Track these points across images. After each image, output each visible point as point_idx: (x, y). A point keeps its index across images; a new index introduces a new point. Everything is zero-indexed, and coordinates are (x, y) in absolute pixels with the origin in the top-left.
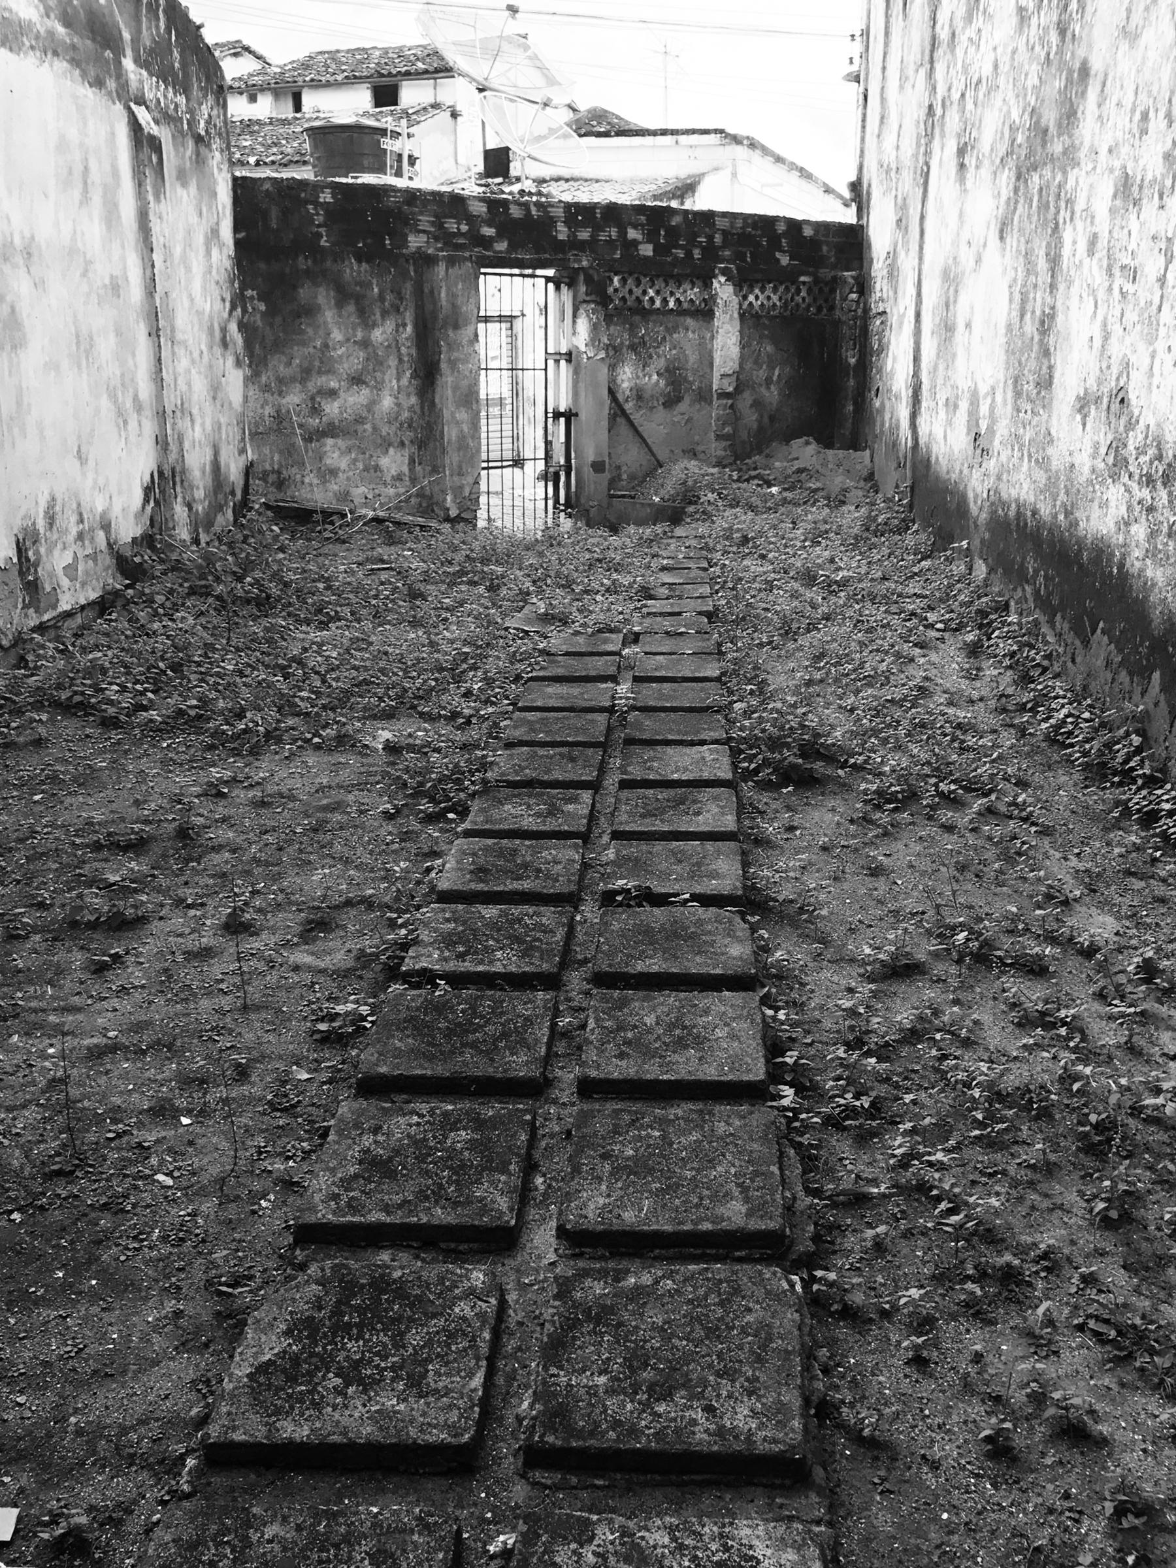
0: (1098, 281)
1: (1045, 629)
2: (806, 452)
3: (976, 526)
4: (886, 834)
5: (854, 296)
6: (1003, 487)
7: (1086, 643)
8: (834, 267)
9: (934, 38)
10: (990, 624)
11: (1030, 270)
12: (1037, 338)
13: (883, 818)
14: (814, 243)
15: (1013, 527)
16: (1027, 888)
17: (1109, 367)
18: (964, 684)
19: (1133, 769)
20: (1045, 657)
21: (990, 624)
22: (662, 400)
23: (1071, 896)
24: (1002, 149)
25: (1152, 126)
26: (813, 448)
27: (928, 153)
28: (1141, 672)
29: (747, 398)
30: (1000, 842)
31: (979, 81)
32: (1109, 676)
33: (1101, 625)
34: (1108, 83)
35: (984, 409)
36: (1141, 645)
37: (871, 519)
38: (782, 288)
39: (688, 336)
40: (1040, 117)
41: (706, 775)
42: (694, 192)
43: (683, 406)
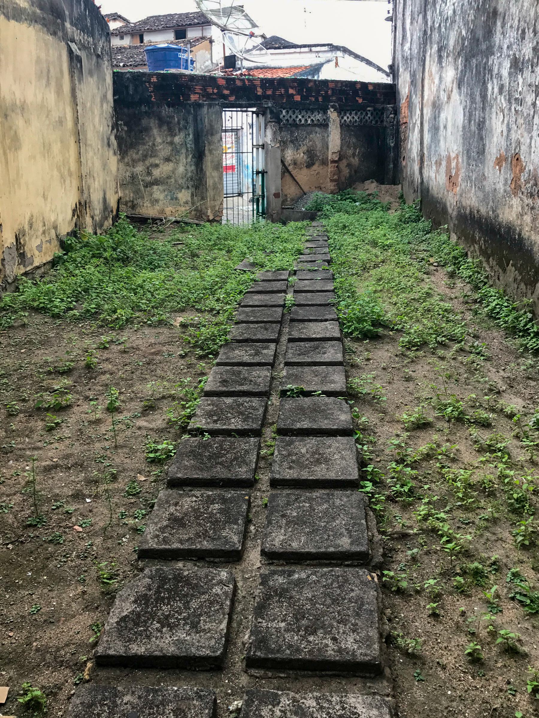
0: (504, 105)
1: (485, 264)
2: (372, 186)
3: (451, 218)
4: (412, 362)
5: (392, 116)
6: (463, 200)
7: (504, 271)
8: (383, 103)
12: (477, 132)
13: (411, 354)
14: (374, 93)
15: (469, 218)
16: (480, 386)
17: (511, 144)
18: (447, 291)
19: (528, 329)
21: (459, 263)
22: (305, 165)
23: (501, 389)
24: (458, 48)
26: (375, 184)
27: (425, 52)
29: (344, 162)
32: (516, 286)
33: (511, 262)
35: (453, 164)
38: (359, 113)
39: (316, 137)
40: (475, 33)
41: (328, 335)
43: (315, 167)
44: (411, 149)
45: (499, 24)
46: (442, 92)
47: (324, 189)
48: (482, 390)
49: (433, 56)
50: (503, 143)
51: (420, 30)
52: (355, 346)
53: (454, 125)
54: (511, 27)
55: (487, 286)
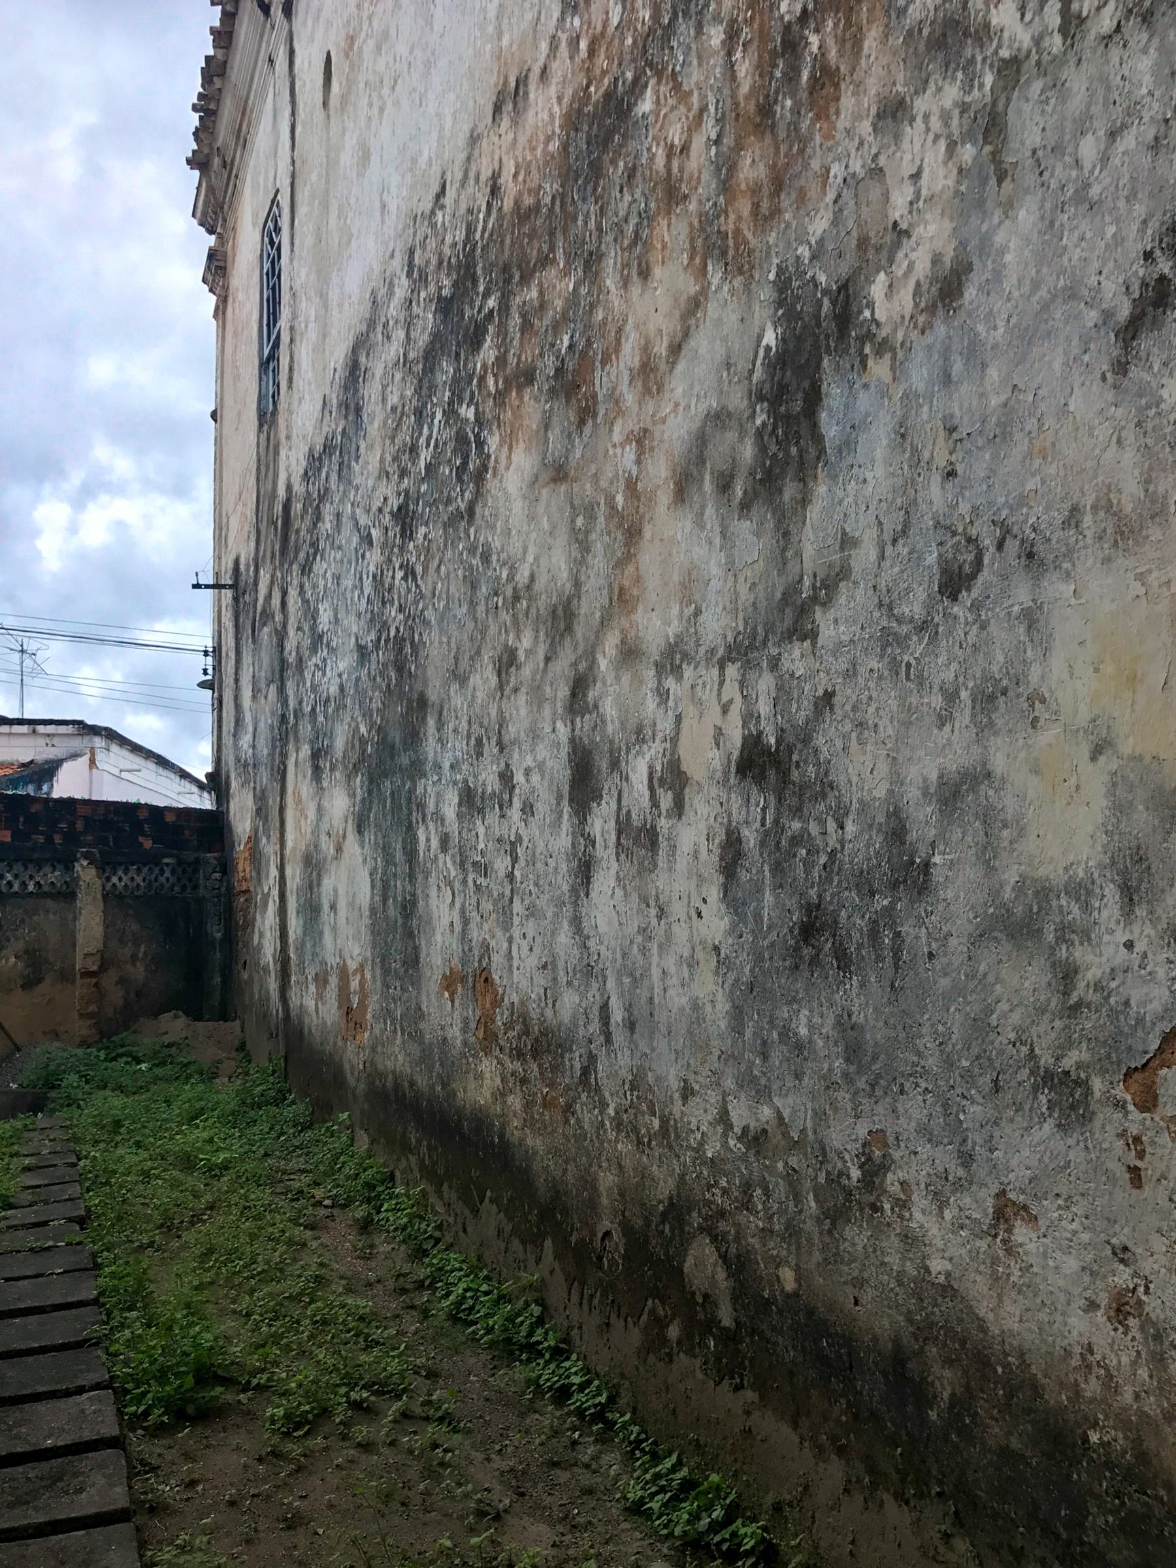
0: (453, 874)
1: (433, 1199)
2: (175, 1026)
3: (355, 1097)
4: (298, 1470)
5: (217, 875)
6: (378, 1059)
7: (476, 1212)
9: (283, 661)
11: (389, 860)
12: (400, 921)
13: (294, 1449)
17: (470, 950)
18: (359, 1265)
19: (539, 1343)
22: (20, 983)
23: (501, 1506)
24: (354, 757)
26: (182, 1020)
27: (284, 756)
28: (533, 1240)
29: (112, 975)
30: (421, 1455)
31: (328, 700)
32: (503, 1246)
33: (488, 1193)
35: (354, 984)
41: (87, 1435)
43: (44, 987)
44: (260, 946)
45: (431, 722)
46: (324, 838)
48: (461, 1518)
50: (456, 947)
51: (273, 714)
53: (351, 905)
54: (455, 730)
55: (441, 1246)
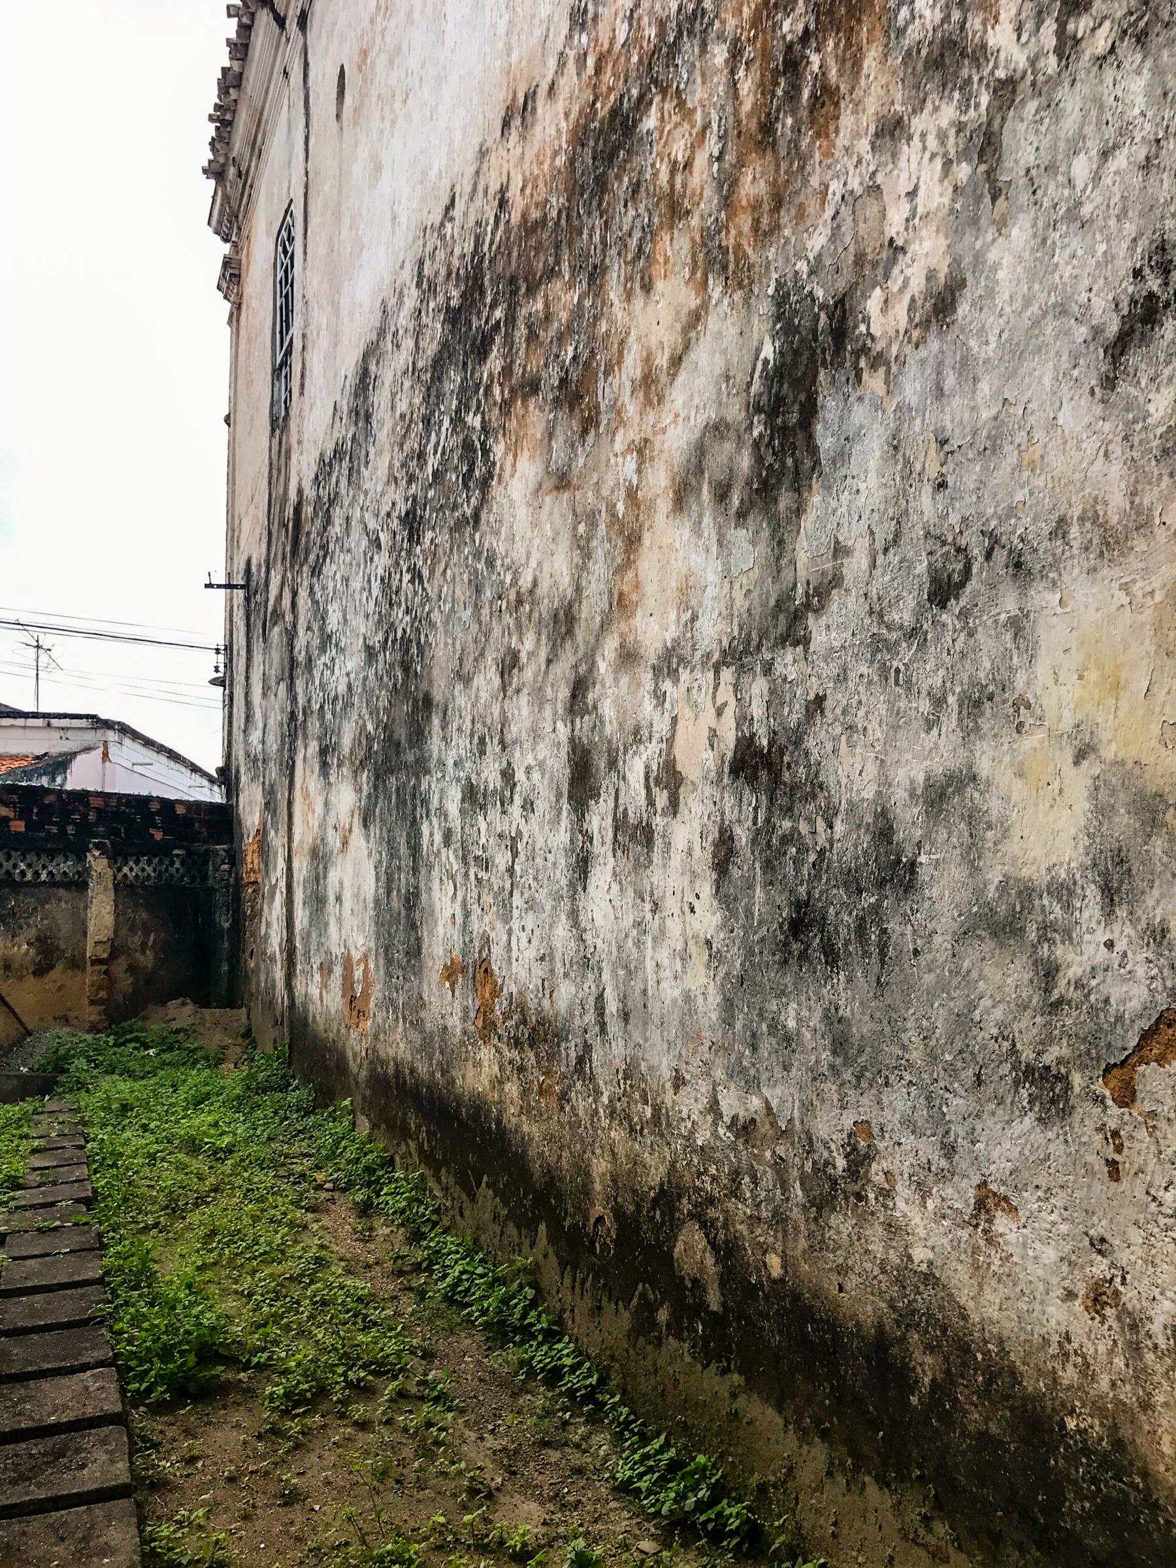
0: (455, 867)
2: (182, 1013)
3: (357, 1083)
4: (298, 1446)
5: (226, 867)
7: (472, 1197)
8: (206, 842)
10: (377, 1181)
11: (393, 853)
12: (403, 913)
13: (293, 1427)
14: (186, 821)
15: (393, 1084)
16: (448, 1486)
17: (471, 941)
19: (532, 1325)
20: (434, 1212)
21: (377, 1181)
23: (493, 1485)
24: (361, 754)
25: (489, 749)
26: (190, 1008)
27: (293, 751)
28: (527, 1225)
29: (122, 963)
30: (416, 1433)
33: (485, 1178)
34: (449, 712)
35: (358, 974)
36: (525, 1197)
37: (251, 1077)
38: (156, 861)
39: (60, 907)
40: (392, 732)
41: (90, 1411)
42: (65, 769)
43: (53, 974)
44: (267, 936)
45: (436, 721)
47: (75, 1022)
49: (309, 761)
51: (282, 711)
52: (154, 1426)
53: (356, 896)
54: (459, 729)
55: (438, 1229)
